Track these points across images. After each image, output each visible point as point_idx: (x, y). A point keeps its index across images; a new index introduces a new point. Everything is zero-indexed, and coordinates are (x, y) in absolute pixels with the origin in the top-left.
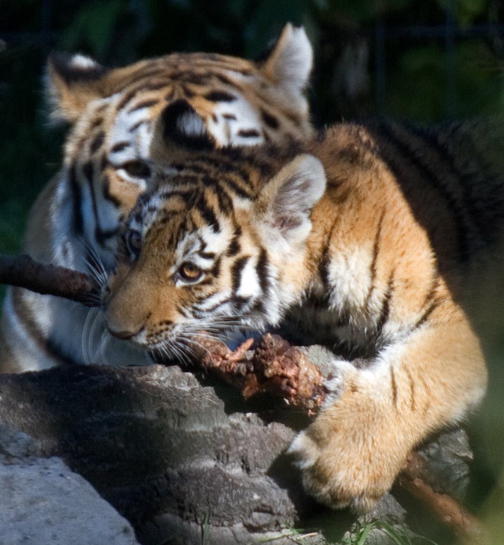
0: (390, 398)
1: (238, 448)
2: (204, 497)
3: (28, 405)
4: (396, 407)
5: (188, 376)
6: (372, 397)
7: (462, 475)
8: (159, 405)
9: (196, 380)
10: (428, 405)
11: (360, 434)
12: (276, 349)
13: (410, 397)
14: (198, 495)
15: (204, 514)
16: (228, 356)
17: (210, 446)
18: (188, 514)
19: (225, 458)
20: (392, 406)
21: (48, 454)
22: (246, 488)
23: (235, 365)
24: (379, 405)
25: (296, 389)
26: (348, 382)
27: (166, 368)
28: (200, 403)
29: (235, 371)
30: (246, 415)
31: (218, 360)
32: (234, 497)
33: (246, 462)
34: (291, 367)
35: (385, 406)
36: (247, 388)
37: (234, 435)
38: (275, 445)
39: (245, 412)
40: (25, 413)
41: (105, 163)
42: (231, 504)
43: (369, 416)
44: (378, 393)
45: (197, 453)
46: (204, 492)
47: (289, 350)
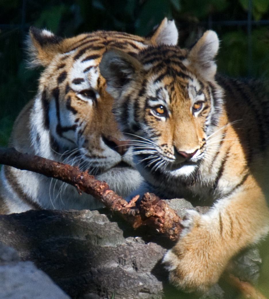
0: (219, 230)
1: (130, 257)
2: (112, 284)
3: (13, 232)
4: (222, 236)
5: (103, 216)
6: (208, 230)
7: (256, 272)
8: (87, 233)
9: (107, 218)
10: (240, 235)
11: (201, 252)
12: (152, 201)
13: (230, 229)
14: (109, 283)
15: (112, 293)
16: (125, 205)
17: (115, 255)
18: (103, 293)
19: (124, 262)
20: (220, 235)
21: (24, 259)
22: (135, 279)
23: (129, 210)
24: (212, 234)
25: (163, 224)
26: (195, 222)
27: (91, 212)
28: (110, 232)
29: (129, 213)
30: (135, 238)
31: (120, 207)
32: (128, 284)
33: (135, 265)
34: (160, 211)
35: (215, 235)
36: (136, 223)
37: (128, 249)
38: (151, 255)
39: (135, 237)
40: (12, 237)
41: (68, 88)
42: (127, 288)
43: (206, 241)
44: (212, 228)
45: (108, 259)
46: (112, 281)
47: (159, 202)
